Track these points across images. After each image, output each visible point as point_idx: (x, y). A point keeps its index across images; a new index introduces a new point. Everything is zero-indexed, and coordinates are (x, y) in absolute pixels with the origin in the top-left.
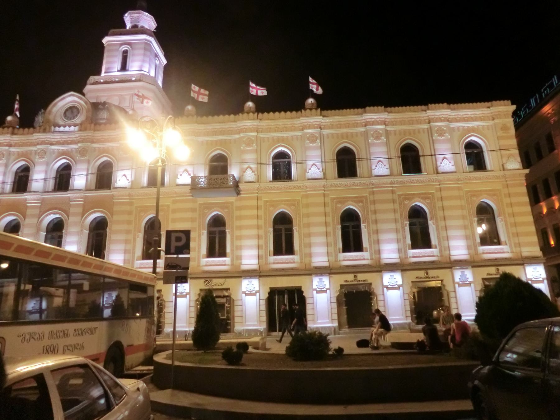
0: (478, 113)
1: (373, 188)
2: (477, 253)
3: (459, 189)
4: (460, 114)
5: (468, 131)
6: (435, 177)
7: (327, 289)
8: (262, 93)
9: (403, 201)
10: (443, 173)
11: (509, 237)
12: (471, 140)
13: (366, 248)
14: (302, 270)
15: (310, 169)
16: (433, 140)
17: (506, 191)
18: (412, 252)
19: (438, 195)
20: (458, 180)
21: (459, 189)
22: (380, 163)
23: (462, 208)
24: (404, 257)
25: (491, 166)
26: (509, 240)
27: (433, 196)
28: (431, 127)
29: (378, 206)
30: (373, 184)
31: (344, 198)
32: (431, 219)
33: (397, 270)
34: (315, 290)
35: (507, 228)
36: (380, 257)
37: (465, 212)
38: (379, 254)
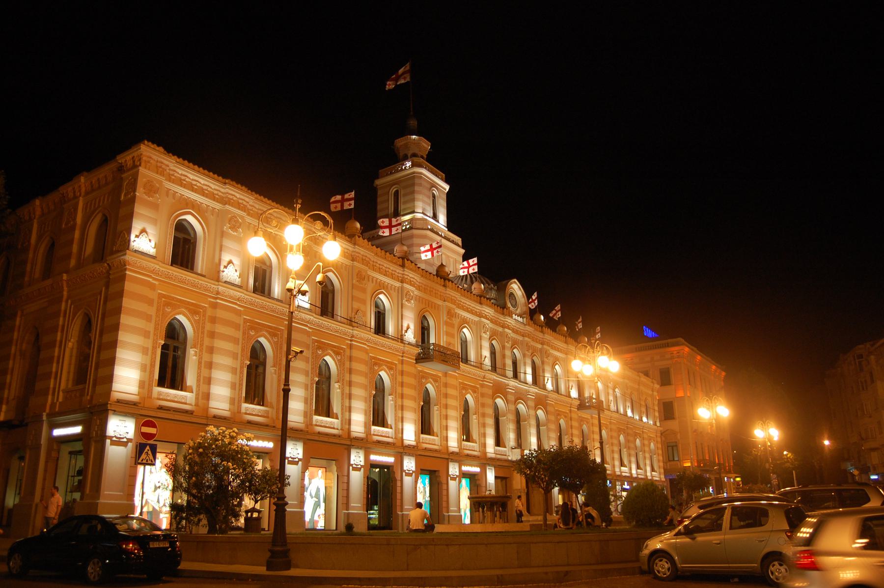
0: (213, 186)
1: (216, 298)
2: (150, 395)
3: (366, 351)
4: (189, 175)
5: (187, 204)
6: (347, 329)
7: (300, 460)
8: (383, 222)
9: (164, 306)
10: (226, 282)
11: (198, 380)
12: (185, 220)
13: (191, 387)
14: (197, 417)
15: (225, 267)
16: (402, 304)
17: (399, 367)
18: (246, 406)
19: (210, 312)
20: (153, 271)
21: (366, 351)
22: (144, 234)
23: (235, 341)
24: (236, 410)
25: (202, 268)
26: (198, 386)
27: (205, 311)
28: (402, 287)
29: (220, 329)
30: (218, 293)
31: (259, 324)
32: (194, 346)
33: (412, 456)
34: (111, 438)
35: (199, 368)
36: (349, 429)
37: (150, 327)
38: (350, 424)
